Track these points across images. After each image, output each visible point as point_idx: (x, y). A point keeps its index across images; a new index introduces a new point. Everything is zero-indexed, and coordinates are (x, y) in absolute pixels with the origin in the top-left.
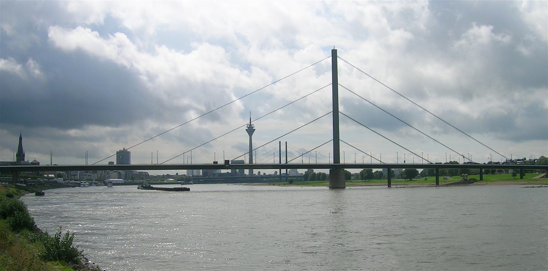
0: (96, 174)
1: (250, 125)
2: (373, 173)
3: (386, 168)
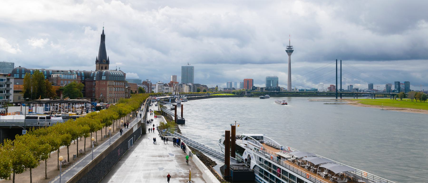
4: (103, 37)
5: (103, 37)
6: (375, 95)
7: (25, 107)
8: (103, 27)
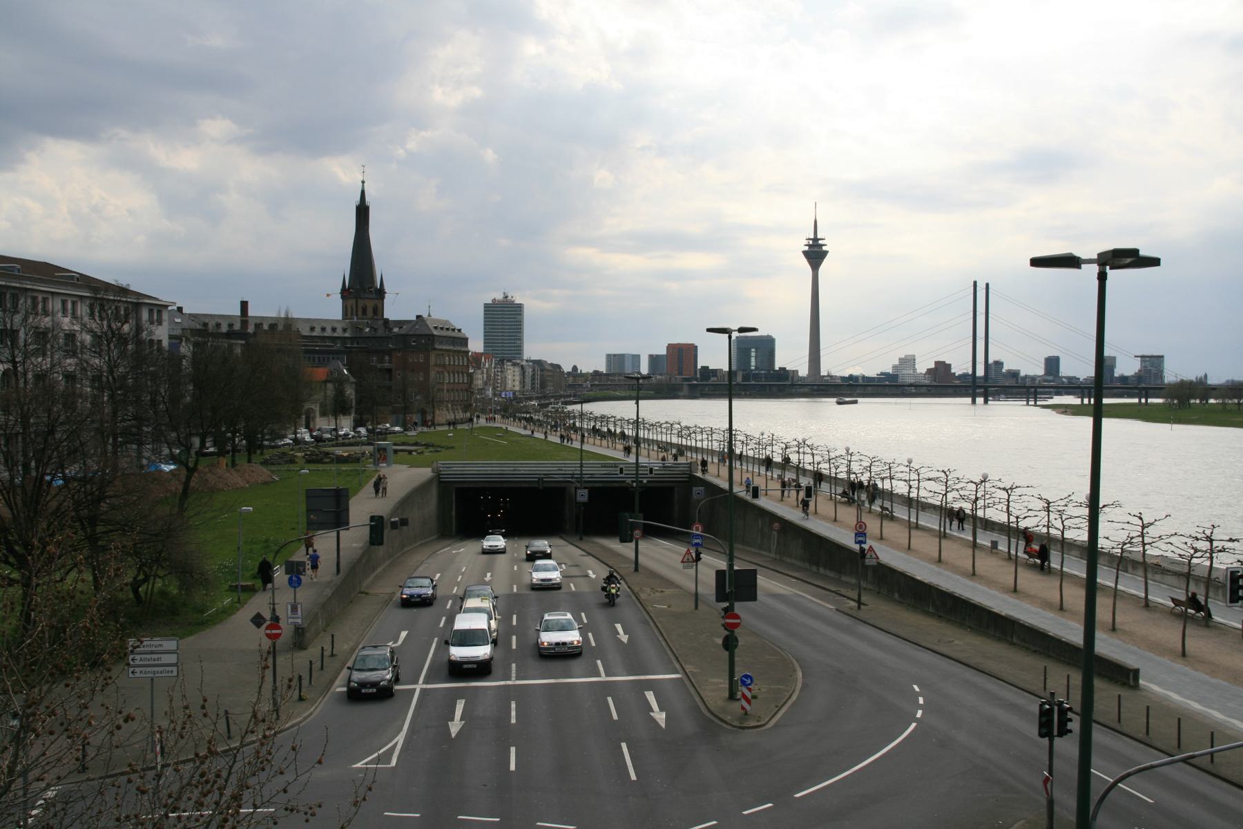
0: (480, 371)
1: (816, 239)
4: (362, 212)
5: (362, 212)
6: (1083, 391)
7: (725, 403)
8: (363, 182)
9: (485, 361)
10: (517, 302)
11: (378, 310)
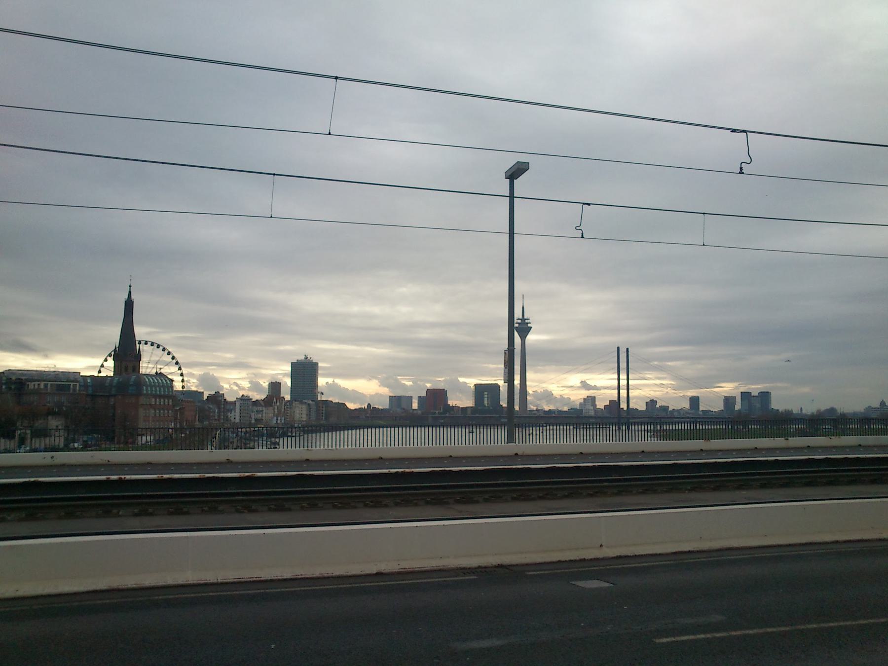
0: (272, 408)
2: (331, 384)
3: (507, 404)
8: (130, 286)
9: (277, 401)
10: (314, 361)
11: (136, 368)
